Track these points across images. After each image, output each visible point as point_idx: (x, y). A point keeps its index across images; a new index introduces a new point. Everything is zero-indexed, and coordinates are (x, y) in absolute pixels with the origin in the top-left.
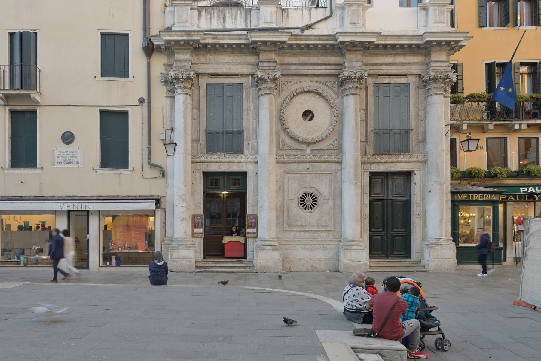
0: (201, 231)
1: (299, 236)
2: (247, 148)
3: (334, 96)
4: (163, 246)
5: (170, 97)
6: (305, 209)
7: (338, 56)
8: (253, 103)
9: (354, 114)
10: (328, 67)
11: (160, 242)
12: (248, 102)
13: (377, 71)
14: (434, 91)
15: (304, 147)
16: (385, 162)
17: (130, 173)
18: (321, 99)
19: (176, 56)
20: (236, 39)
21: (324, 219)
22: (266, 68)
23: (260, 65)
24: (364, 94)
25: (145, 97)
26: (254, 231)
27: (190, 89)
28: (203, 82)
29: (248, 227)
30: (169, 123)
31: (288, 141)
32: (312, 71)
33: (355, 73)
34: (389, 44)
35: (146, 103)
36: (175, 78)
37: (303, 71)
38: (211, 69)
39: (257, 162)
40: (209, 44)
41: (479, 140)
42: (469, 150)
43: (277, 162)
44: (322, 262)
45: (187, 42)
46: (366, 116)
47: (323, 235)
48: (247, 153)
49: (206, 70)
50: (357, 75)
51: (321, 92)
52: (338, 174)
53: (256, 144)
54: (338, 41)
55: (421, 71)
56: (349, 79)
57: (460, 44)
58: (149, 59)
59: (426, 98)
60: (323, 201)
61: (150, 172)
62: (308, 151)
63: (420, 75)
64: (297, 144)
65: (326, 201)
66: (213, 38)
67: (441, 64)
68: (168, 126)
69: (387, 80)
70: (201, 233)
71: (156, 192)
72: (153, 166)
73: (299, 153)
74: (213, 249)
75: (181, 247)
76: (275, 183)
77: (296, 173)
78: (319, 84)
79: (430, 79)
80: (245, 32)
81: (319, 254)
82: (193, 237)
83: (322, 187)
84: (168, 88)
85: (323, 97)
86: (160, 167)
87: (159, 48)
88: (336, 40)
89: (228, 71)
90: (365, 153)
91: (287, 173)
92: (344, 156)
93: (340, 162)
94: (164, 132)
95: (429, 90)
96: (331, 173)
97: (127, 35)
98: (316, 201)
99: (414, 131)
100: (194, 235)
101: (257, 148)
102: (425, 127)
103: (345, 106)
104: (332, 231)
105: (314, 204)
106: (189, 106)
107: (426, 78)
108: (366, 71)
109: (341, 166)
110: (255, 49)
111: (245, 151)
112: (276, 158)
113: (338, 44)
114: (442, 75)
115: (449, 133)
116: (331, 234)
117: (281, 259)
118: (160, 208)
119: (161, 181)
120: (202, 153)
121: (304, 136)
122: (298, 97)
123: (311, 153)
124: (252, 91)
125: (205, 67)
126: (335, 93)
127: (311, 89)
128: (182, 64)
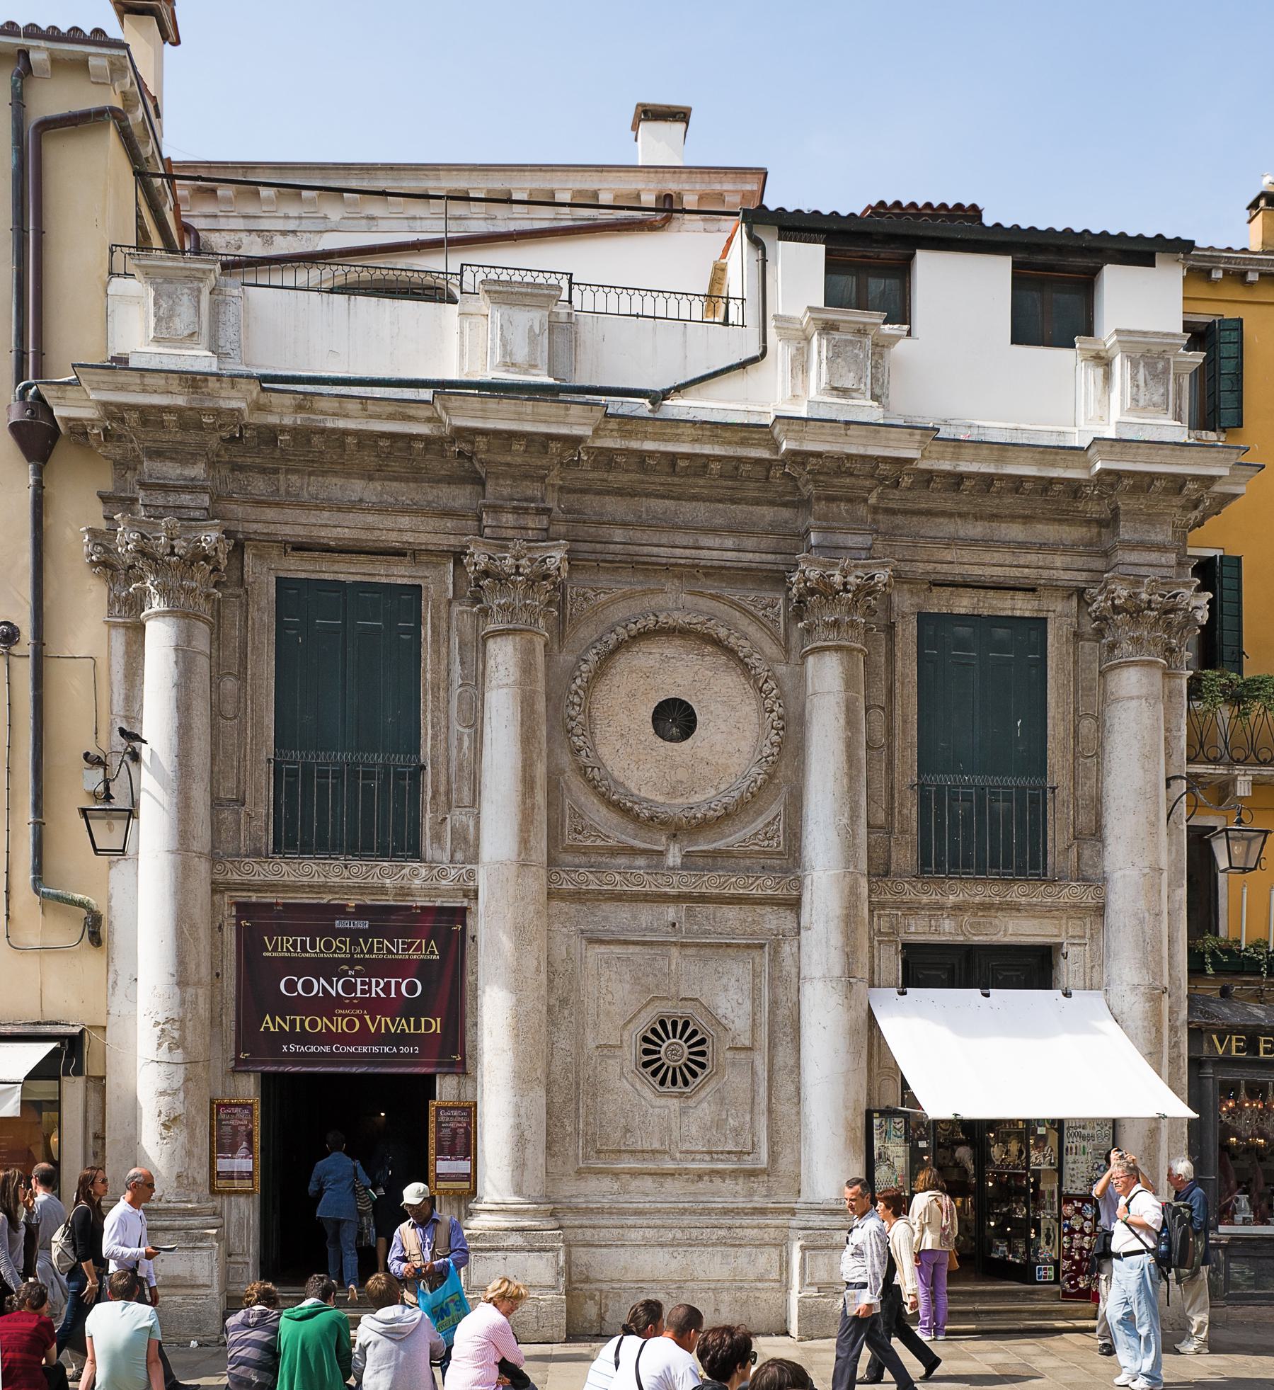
1: (643, 1192)
2: (437, 838)
3: (771, 649)
6: (662, 1083)
8: (462, 663)
9: (842, 721)
10: (750, 542)
12: (437, 664)
15: (660, 841)
20: (391, 417)
22: (510, 533)
23: (487, 520)
24: (883, 650)
26: (463, 1166)
28: (263, 576)
29: (440, 1151)
31: (599, 814)
34: (970, 476)
37: (655, 550)
38: (295, 524)
39: (476, 892)
40: (283, 429)
41: (1266, 832)
42: (1231, 867)
45: (188, 420)
48: (438, 855)
49: (272, 528)
50: (851, 579)
51: (723, 633)
52: (786, 949)
53: (471, 824)
55: (1084, 575)
56: (825, 591)
57: (1218, 488)
60: (729, 1055)
61: (34, 924)
62: (674, 857)
63: (1080, 592)
64: (631, 827)
65: (743, 1055)
66: (300, 408)
67: (1153, 557)
76: (543, 976)
77: (626, 943)
78: (714, 604)
79: (1116, 609)
80: (426, 394)
82: (214, 1192)
83: (729, 999)
85: (730, 652)
87: (79, 430)
88: (777, 447)
89: (363, 535)
90: (880, 871)
91: (591, 941)
92: (808, 881)
93: (795, 905)
95: (1112, 647)
96: (762, 946)
100: (218, 1184)
101: (477, 838)
102: (1099, 781)
104: (763, 1171)
105: (696, 1066)
106: (203, 664)
107: (1100, 603)
108: (883, 565)
109: (798, 916)
110: (470, 459)
112: (549, 880)
113: (783, 463)
114: (1156, 597)
115: (1183, 808)
116: (759, 1186)
118: (78, 1072)
119: (91, 960)
121: (660, 799)
123: (684, 867)
125: (270, 514)
126: (774, 638)
127: (680, 619)
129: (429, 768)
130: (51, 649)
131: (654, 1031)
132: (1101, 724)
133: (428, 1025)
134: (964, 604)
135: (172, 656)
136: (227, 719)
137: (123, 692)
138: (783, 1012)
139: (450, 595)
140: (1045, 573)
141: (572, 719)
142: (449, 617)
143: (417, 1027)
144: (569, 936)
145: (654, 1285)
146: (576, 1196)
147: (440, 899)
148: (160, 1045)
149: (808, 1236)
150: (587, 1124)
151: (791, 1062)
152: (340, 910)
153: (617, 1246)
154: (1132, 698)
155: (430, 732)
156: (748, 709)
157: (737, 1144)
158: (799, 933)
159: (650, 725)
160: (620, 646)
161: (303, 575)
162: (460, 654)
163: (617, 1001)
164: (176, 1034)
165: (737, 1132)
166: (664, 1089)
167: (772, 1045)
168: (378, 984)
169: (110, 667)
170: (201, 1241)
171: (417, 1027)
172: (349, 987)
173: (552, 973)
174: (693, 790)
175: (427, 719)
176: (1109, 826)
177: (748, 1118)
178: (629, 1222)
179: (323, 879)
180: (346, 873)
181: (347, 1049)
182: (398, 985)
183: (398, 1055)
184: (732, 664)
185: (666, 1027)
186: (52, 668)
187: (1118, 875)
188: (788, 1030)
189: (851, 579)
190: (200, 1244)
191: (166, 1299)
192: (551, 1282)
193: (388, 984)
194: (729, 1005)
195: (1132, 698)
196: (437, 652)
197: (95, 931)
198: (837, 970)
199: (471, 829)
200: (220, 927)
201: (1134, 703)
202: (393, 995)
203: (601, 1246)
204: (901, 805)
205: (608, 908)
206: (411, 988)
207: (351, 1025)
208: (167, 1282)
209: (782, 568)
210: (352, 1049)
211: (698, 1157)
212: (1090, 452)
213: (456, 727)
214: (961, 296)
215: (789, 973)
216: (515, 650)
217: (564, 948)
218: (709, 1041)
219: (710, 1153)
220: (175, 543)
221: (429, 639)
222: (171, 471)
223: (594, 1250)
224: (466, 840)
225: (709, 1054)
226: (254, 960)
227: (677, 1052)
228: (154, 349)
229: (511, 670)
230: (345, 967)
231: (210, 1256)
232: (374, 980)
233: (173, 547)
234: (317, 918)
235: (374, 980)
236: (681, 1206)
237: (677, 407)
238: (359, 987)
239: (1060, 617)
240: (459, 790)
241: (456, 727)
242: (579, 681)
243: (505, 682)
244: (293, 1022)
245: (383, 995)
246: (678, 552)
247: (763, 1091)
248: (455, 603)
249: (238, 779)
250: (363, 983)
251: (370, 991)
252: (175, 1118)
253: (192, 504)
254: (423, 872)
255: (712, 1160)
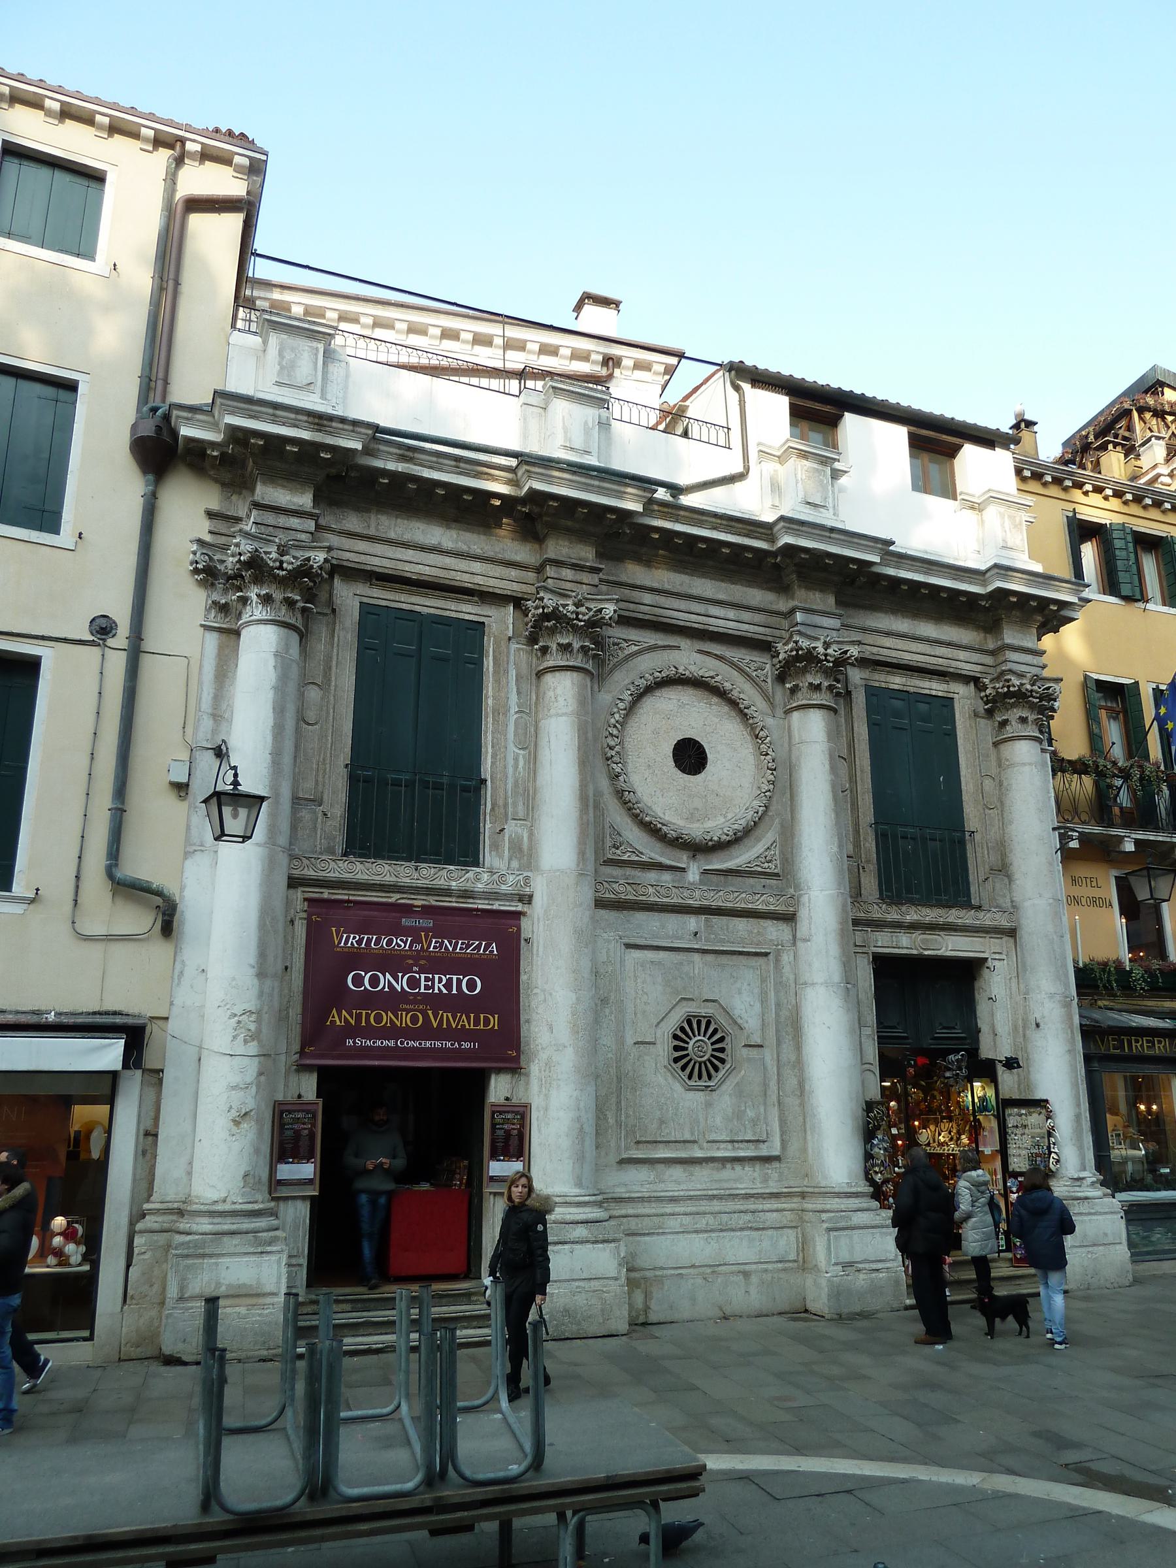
0: (307, 1170)
1: (676, 1181)
2: (495, 846)
4: (138, 1241)
5: (220, 630)
7: (770, 589)
8: (519, 693)
10: (746, 616)
11: (124, 1221)
13: (875, 650)
14: (1014, 728)
16: (914, 927)
17: (18, 909)
18: (726, 709)
19: (259, 489)
21: (750, 1113)
22: (569, 586)
25: (123, 619)
27: (304, 610)
30: (207, 723)
31: (633, 835)
32: (700, 619)
33: (827, 645)
35: (124, 637)
36: (248, 565)
38: (380, 558)
39: (531, 897)
43: (600, 904)
44: (754, 1279)
45: (309, 450)
46: (853, 779)
47: (747, 1179)
49: (362, 559)
51: (727, 685)
52: (786, 958)
53: (526, 835)
54: (781, 543)
55: (979, 668)
56: (810, 658)
58: (156, 486)
59: (996, 744)
60: (745, 1051)
61: (105, 913)
62: (693, 875)
64: (658, 845)
65: (754, 1053)
68: (204, 734)
69: (897, 681)
70: (310, 1182)
71: (127, 997)
72: (128, 889)
73: (667, 877)
74: (344, 1249)
75: (230, 1243)
78: (718, 663)
80: (513, 462)
81: (740, 1249)
83: (742, 1001)
84: (216, 596)
85: (733, 704)
86: (159, 893)
87: (197, 449)
88: (772, 539)
90: (856, 894)
91: (629, 946)
92: (805, 899)
93: (789, 918)
94: (185, 756)
95: (1004, 723)
96: (766, 954)
97: (71, 387)
98: (722, 1050)
99: (977, 837)
101: (530, 848)
103: (796, 739)
111: (489, 857)
116: (772, 1170)
117: (623, 1280)
118: (138, 1065)
119: (159, 949)
120: (331, 851)
121: (681, 823)
122: (658, 693)
123: (701, 882)
124: (518, 656)
125: (362, 546)
128: (283, 521)
129: (489, 783)
130: (149, 644)
131: (682, 1029)
132: (1001, 785)
133: (487, 1022)
134: (897, 681)
135: (271, 662)
136: (309, 724)
137: (212, 691)
138: (784, 1013)
139: (510, 634)
140: (954, 664)
141: (611, 748)
142: (508, 652)
143: (477, 1023)
144: (609, 941)
145: (691, 1271)
146: (618, 1186)
147: (497, 903)
148: (235, 1037)
149: (831, 1219)
150: (627, 1116)
151: (793, 1058)
152: (407, 910)
153: (658, 1234)
154: (1024, 764)
155: (490, 750)
156: (746, 750)
157: (754, 1134)
158: (794, 944)
159: (671, 759)
160: (649, 690)
161: (384, 603)
162: (517, 685)
163: (652, 1001)
164: (253, 1027)
165: (754, 1122)
166: (691, 1083)
167: (779, 1043)
168: (440, 981)
169: (201, 667)
170: (270, 1244)
171: (477, 1023)
172: (414, 983)
173: (596, 974)
174: (706, 817)
175: (488, 739)
176: (1015, 864)
177: (762, 1110)
178: (668, 1210)
179: (394, 879)
180: (416, 875)
181: (411, 1043)
182: (459, 982)
183: (459, 1050)
184: (733, 714)
185: (692, 1025)
186: (146, 661)
187: (1027, 904)
188: (790, 1029)
189: (830, 651)
190: (269, 1249)
191: (228, 1310)
192: (613, 1274)
193: (450, 981)
194: (742, 1007)
195: (1024, 764)
196: (497, 681)
197: (168, 920)
198: (837, 976)
199: (526, 839)
200: (292, 922)
201: (1027, 769)
202: (454, 991)
203: (644, 1234)
204: (865, 839)
205: (641, 916)
206: (471, 985)
207: (414, 1020)
208: (231, 1293)
209: (770, 639)
210: (416, 1044)
211: (723, 1146)
212: (988, 575)
213: (512, 748)
214: (875, 448)
215: (788, 979)
216: (573, 683)
217: (604, 951)
218: (728, 1039)
219: (732, 1142)
220: (285, 558)
221: (491, 669)
222: (281, 496)
223: (638, 1238)
224: (521, 850)
225: (728, 1051)
226: (321, 955)
227: (701, 1050)
228: (276, 389)
229: (570, 701)
230: (411, 962)
231: (279, 1262)
232: (437, 977)
233: (281, 562)
234: (387, 916)
235: (437, 977)
236: (710, 1193)
237: (687, 500)
238: (423, 983)
239: (964, 698)
240: (515, 804)
241: (512, 748)
242: (617, 716)
243: (564, 710)
244: (359, 1016)
245: (445, 991)
246: (693, 617)
247: (773, 1084)
248: (513, 640)
249: (317, 781)
250: (427, 979)
251: (433, 987)
252: (246, 1114)
253: (300, 528)
254: (485, 876)
255: (734, 1149)
